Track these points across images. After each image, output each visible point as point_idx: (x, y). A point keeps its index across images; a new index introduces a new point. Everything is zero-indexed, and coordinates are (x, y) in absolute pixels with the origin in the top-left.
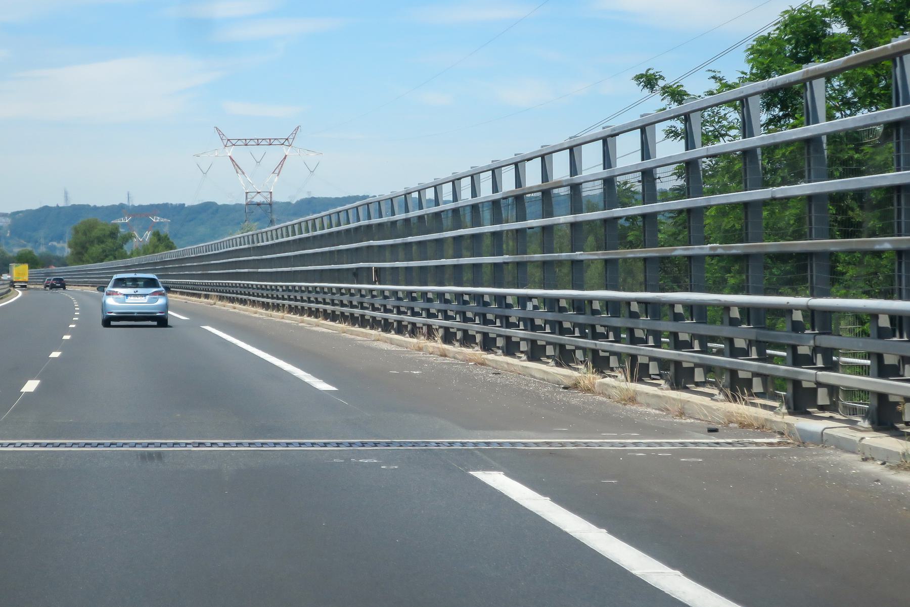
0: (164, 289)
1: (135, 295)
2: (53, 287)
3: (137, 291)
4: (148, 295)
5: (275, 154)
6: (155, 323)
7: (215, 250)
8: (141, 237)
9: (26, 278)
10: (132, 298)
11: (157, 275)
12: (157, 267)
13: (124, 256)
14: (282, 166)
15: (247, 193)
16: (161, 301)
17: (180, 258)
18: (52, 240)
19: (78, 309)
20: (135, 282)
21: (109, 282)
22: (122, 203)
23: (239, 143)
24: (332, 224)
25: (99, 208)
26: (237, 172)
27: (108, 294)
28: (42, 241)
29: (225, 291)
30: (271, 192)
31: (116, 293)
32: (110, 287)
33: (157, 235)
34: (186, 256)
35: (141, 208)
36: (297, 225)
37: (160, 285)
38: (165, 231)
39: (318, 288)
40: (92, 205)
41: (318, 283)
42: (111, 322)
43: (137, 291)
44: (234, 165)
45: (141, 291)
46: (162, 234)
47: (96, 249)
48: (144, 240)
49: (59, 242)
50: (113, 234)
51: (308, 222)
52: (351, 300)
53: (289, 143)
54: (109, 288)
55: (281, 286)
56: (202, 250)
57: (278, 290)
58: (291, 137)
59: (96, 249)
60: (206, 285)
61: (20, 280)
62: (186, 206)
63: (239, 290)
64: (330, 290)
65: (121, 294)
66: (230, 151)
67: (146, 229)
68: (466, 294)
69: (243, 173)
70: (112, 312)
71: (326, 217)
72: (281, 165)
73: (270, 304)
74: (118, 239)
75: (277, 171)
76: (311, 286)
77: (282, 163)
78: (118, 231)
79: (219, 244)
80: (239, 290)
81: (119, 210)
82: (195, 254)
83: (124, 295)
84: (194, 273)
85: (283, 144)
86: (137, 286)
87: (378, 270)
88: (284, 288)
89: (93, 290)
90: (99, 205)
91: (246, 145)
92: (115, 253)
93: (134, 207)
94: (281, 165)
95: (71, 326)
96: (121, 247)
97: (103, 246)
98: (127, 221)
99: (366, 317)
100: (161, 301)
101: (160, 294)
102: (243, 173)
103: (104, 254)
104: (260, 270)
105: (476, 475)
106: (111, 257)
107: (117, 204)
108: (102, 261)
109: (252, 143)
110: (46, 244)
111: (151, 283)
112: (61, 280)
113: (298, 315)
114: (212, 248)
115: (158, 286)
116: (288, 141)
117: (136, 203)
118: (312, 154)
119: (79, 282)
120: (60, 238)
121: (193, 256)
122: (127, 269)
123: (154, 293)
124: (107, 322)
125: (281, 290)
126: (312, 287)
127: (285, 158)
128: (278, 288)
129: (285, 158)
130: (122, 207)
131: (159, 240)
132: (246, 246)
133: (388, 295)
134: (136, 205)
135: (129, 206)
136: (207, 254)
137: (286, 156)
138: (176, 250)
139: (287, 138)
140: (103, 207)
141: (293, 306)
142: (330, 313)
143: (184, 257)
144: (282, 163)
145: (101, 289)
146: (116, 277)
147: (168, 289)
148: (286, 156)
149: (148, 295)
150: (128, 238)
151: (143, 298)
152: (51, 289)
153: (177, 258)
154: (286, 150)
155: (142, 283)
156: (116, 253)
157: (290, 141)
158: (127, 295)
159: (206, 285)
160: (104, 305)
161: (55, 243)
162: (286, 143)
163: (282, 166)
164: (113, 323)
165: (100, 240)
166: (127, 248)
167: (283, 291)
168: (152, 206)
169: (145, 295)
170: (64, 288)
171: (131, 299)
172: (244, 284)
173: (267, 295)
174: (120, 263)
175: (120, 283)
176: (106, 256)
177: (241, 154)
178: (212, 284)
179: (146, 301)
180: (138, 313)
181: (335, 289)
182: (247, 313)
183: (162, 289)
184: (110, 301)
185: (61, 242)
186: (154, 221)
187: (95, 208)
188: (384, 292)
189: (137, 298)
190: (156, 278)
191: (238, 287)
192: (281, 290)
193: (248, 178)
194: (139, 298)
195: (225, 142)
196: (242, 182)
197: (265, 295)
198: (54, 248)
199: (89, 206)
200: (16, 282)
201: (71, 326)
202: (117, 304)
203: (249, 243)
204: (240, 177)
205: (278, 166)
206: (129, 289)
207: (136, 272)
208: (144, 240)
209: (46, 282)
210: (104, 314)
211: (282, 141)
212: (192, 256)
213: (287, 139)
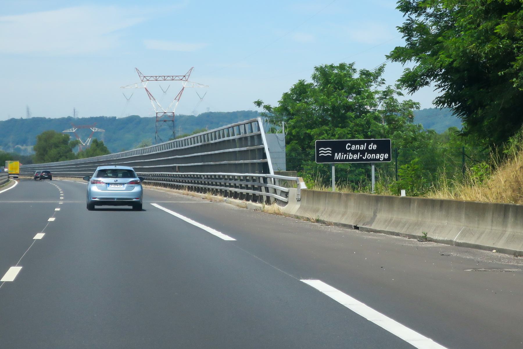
0: (139, 179)
1: (116, 184)
2: (42, 178)
3: (117, 181)
4: (126, 183)
5: (178, 85)
6: (131, 207)
7: (158, 151)
8: (84, 142)
9: (18, 171)
10: (113, 186)
11: (134, 168)
12: (78, 166)
13: (73, 157)
14: (181, 94)
15: (157, 113)
16: (137, 189)
17: (108, 159)
18: (17, 144)
19: (63, 198)
20: (115, 173)
21: (93, 174)
22: (69, 116)
23: (152, 79)
24: (234, 133)
25: (52, 120)
26: (150, 99)
27: (94, 183)
28: (10, 144)
29: (151, 179)
30: (174, 113)
31: (99, 182)
32: (95, 177)
33: (95, 142)
34: (112, 159)
35: (84, 120)
36: (231, 128)
37: (136, 175)
38: (102, 139)
39: (196, 175)
40: (47, 117)
41: (214, 173)
42: (95, 206)
43: (117, 181)
44: (148, 94)
45: (120, 180)
46: (99, 141)
47: (53, 152)
48: (86, 144)
49: (22, 146)
50: (65, 141)
51: (212, 133)
52: (235, 183)
53: (186, 79)
54: (94, 178)
55: (204, 175)
56: (136, 153)
57: (202, 178)
58: (187, 75)
59: (53, 152)
60: (158, 176)
61: (14, 173)
62: (117, 118)
63: (178, 179)
64: (234, 177)
65: (103, 183)
66: (146, 84)
67: (88, 136)
68: (269, 178)
69: (154, 99)
70: (96, 198)
71: (235, 127)
72: (180, 94)
73: (193, 187)
74: (68, 144)
75: (178, 98)
76: (242, 176)
77: (181, 93)
78: (69, 139)
79: (153, 148)
80: (178, 179)
81: (67, 122)
82: (201, 142)
83: (106, 183)
84: (212, 163)
85: (182, 80)
86: (117, 177)
87: (179, 167)
88: (206, 177)
89: (81, 181)
90: (52, 117)
91: (157, 80)
92: (67, 154)
93: (79, 119)
94: (180, 94)
95: (56, 209)
96: (71, 151)
97: (58, 149)
98: (74, 131)
99: (250, 194)
100: (137, 189)
101: (135, 183)
102: (154, 99)
103: (59, 155)
104: (144, 167)
105: (232, 238)
106: (64, 157)
107: (66, 117)
108: (57, 160)
109: (160, 78)
110: (14, 147)
111: (128, 174)
112: (49, 172)
113: (175, 189)
114: (135, 153)
115: (134, 177)
116: (185, 78)
117: (80, 117)
118: (201, 87)
119: (74, 174)
120: (24, 142)
121: (115, 159)
122: (108, 162)
123: (132, 183)
124: (92, 206)
125: (203, 178)
126: (243, 176)
127: (183, 89)
128: (202, 176)
129: (183, 89)
130: (69, 119)
131: (97, 145)
132: (200, 144)
133: (218, 177)
134: (80, 117)
135: (75, 119)
136: (122, 158)
137: (184, 88)
138: (110, 155)
139: (184, 75)
140: (55, 119)
141: (223, 190)
142: (224, 191)
143: (142, 155)
144: (181, 93)
145: (87, 178)
146: (99, 168)
147: (142, 179)
148: (184, 88)
149: (126, 183)
150: (75, 144)
151: (122, 186)
152: (40, 179)
153: (106, 160)
154: (184, 84)
155: (121, 175)
156: (68, 154)
157: (187, 77)
158: (109, 184)
159: (158, 176)
160: (89, 193)
161: (20, 146)
162: (184, 79)
163: (181, 94)
164: (96, 207)
165: (56, 146)
166: (76, 151)
167: (205, 178)
168: (92, 119)
169: (123, 184)
170: (51, 179)
171: (112, 187)
172: (184, 175)
173: (212, 183)
174: (103, 157)
175: (103, 173)
176: (61, 157)
177: (153, 86)
178: (147, 175)
179: (124, 189)
180: (118, 199)
181: (213, 176)
182: (162, 191)
183: (137, 179)
184: (94, 188)
185: (24, 145)
186: (93, 131)
187: (50, 120)
188: (253, 177)
189: (116, 186)
190: (133, 170)
191: (167, 177)
192: (203, 178)
193: (158, 103)
194: (119, 186)
195: (142, 78)
196: (154, 106)
197: (187, 181)
198: (19, 150)
199: (45, 118)
200: (10, 174)
201: (56, 209)
202: (100, 191)
203: (201, 142)
204: (152, 102)
205: (178, 95)
206: (110, 178)
207: (115, 165)
208: (86, 144)
209: (35, 174)
210: (89, 198)
211: (181, 78)
212: (114, 159)
213: (184, 76)
